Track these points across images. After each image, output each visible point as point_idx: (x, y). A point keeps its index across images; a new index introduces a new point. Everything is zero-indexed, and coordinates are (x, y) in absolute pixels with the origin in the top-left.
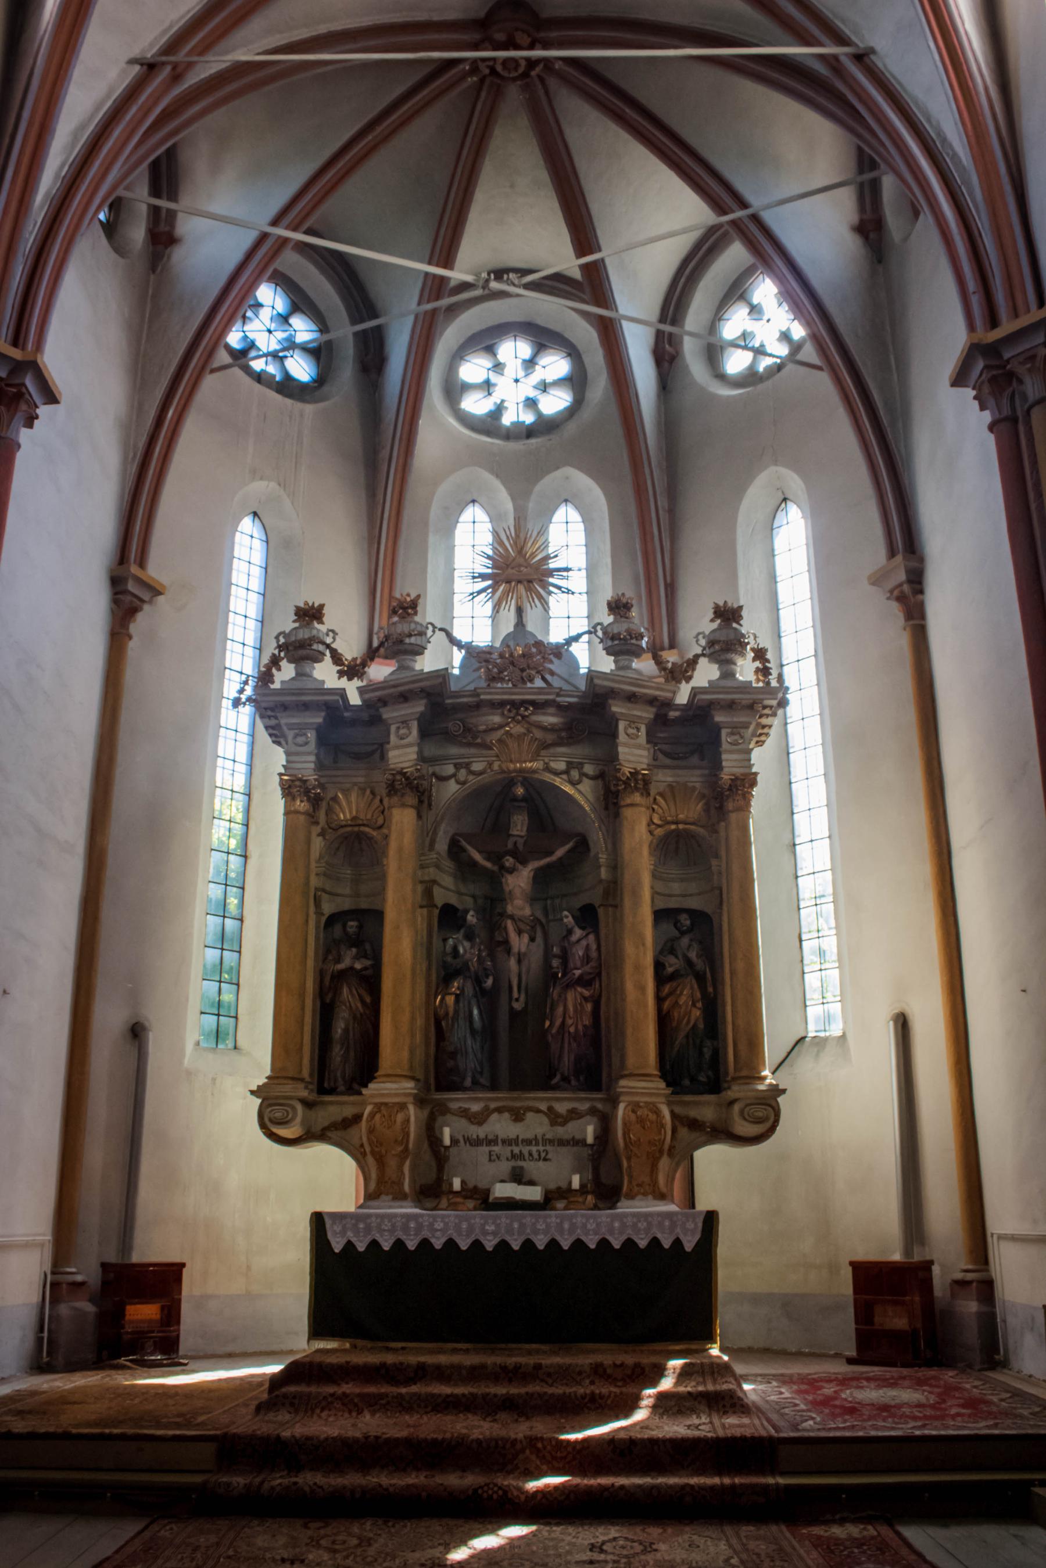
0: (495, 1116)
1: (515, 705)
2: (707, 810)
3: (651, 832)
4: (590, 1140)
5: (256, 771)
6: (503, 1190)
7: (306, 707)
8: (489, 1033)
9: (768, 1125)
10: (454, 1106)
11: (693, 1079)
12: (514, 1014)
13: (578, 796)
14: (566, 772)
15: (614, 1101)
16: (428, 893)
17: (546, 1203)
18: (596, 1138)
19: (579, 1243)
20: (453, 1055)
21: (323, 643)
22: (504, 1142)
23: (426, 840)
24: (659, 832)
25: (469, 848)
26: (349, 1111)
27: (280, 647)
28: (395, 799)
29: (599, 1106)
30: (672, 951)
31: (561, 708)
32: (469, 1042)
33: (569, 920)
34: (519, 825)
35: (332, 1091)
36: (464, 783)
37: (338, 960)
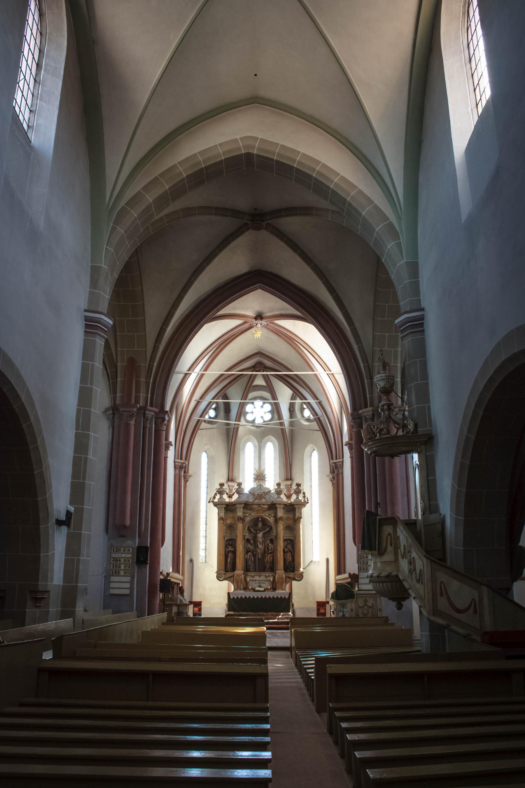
0: (256, 576)
1: (259, 504)
2: (294, 521)
3: (283, 526)
4: (272, 580)
5: (208, 507)
6: (257, 589)
7: (222, 504)
8: (255, 561)
9: (301, 578)
10: (249, 574)
11: (290, 570)
12: (259, 559)
13: (270, 520)
14: (269, 516)
15: (276, 574)
16: (244, 537)
17: (264, 591)
18: (273, 580)
19: (269, 597)
20: (249, 566)
22: (258, 580)
23: (244, 528)
24: (285, 526)
27: (217, 491)
28: (239, 522)
29: (273, 574)
30: (287, 548)
31: (267, 504)
32: (252, 564)
33: (268, 542)
34: (260, 525)
35: (227, 572)
36: (250, 518)
37: (228, 548)
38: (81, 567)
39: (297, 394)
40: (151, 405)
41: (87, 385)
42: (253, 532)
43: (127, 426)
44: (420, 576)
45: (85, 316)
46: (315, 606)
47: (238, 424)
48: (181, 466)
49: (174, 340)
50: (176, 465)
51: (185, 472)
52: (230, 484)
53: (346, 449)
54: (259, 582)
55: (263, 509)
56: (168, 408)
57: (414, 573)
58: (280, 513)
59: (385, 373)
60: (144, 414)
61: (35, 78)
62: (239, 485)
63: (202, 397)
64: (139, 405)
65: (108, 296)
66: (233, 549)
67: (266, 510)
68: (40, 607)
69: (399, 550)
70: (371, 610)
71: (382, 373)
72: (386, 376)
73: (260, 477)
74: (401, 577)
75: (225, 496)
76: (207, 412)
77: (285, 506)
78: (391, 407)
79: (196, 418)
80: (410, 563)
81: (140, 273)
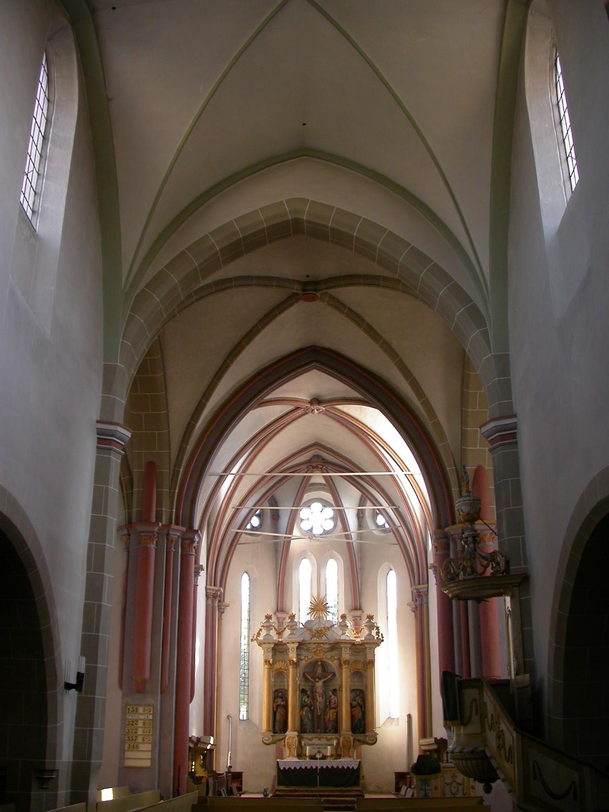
1: (319, 644)
3: (350, 671)
4: (335, 745)
8: (312, 720)
10: (305, 736)
11: (359, 730)
12: (318, 716)
18: (337, 744)
21: (272, 626)
24: (352, 672)
25: (331, 218)
26: (281, 737)
29: (337, 737)
30: (355, 700)
38: (95, 739)
39: (366, 497)
40: (177, 523)
41: (100, 513)
42: (310, 681)
43: (146, 550)
44: (509, 754)
45: (97, 428)
46: (394, 776)
47: (290, 538)
48: (215, 594)
49: (206, 438)
50: (208, 594)
51: (219, 601)
52: (279, 615)
53: (431, 572)
54: (319, 746)
55: (324, 650)
56: (196, 527)
57: (503, 749)
58: (346, 655)
59: (469, 496)
60: (168, 535)
61: (41, 152)
62: (292, 617)
63: (242, 503)
64: (162, 523)
65: (123, 401)
66: (285, 702)
67: (328, 650)
68: (46, 788)
69: (486, 720)
70: (461, 787)
71: (465, 497)
72: (470, 500)
73: (319, 607)
74: (488, 754)
75: (273, 633)
76: (249, 521)
77: (352, 646)
78: (477, 538)
79: (234, 530)
80: (499, 737)
81: (162, 357)
